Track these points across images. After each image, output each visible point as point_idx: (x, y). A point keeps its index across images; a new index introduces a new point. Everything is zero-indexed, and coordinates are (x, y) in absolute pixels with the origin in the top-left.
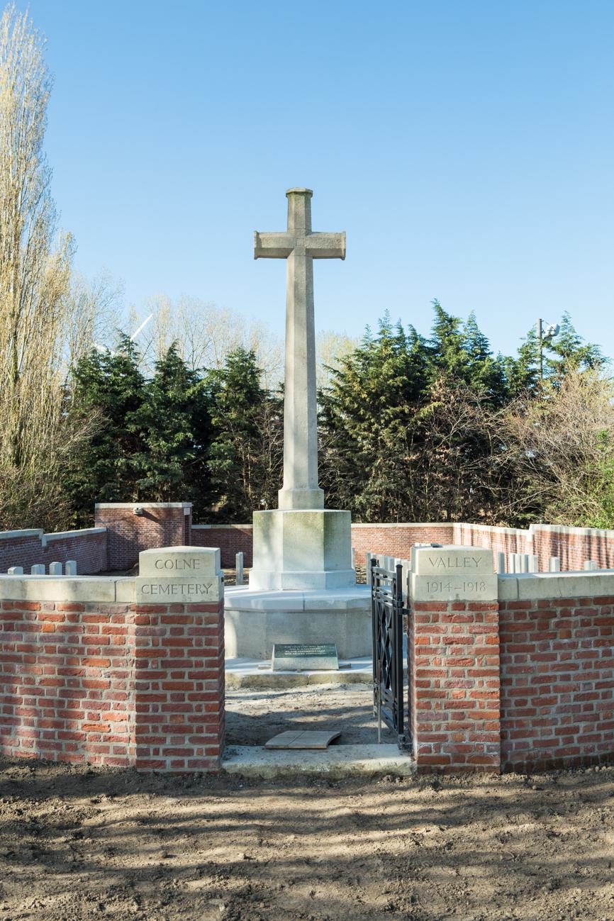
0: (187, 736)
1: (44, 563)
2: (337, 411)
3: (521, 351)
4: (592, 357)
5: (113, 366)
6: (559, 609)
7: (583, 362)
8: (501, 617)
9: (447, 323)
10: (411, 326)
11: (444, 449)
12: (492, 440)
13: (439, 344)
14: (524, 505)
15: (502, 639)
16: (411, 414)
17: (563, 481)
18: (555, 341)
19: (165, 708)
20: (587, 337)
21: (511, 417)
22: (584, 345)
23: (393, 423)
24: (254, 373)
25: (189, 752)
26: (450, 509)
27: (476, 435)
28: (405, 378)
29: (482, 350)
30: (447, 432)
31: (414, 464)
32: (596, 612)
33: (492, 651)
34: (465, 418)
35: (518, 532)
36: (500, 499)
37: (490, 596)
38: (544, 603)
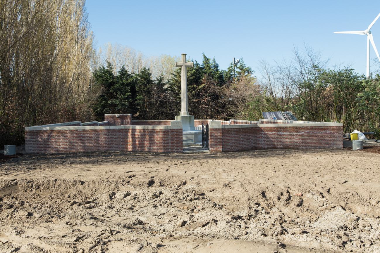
0: (178, 148)
1: (4, 146)
2: (174, 86)
3: (228, 69)
4: (249, 70)
5: (106, 72)
6: (230, 130)
7: (246, 72)
8: (222, 131)
9: (206, 60)
10: (196, 60)
11: (205, 98)
12: (220, 95)
13: (204, 66)
14: (229, 114)
15: (222, 134)
16: (196, 87)
17: (240, 107)
18: (239, 65)
19: (175, 144)
20: (248, 64)
21: (225, 89)
22: (247, 67)
23: (191, 90)
24: (149, 75)
25: (179, 150)
26: (207, 115)
27: (215, 94)
28: (194, 77)
29: (217, 68)
30: (206, 93)
31: (197, 102)
32: (235, 130)
33: (221, 135)
34: (212, 89)
35: (226, 122)
36: (222, 113)
37: (221, 127)
38: (228, 129)
